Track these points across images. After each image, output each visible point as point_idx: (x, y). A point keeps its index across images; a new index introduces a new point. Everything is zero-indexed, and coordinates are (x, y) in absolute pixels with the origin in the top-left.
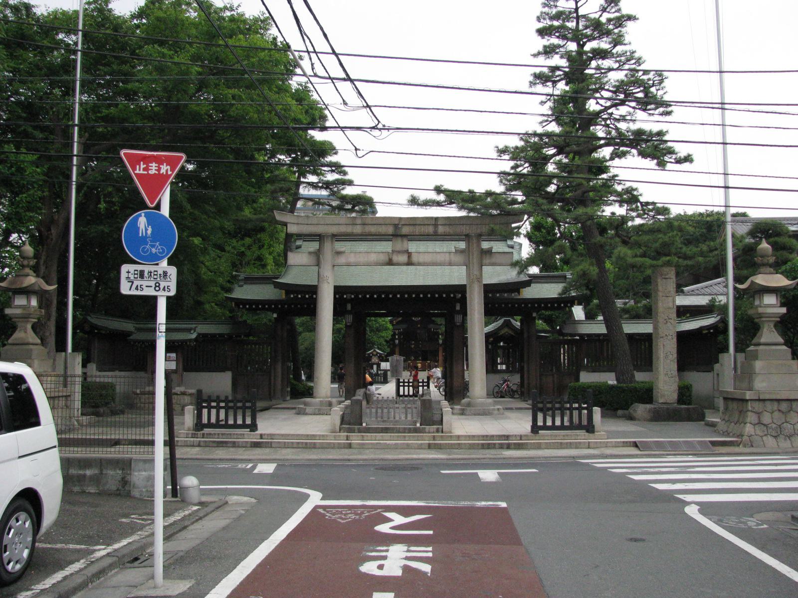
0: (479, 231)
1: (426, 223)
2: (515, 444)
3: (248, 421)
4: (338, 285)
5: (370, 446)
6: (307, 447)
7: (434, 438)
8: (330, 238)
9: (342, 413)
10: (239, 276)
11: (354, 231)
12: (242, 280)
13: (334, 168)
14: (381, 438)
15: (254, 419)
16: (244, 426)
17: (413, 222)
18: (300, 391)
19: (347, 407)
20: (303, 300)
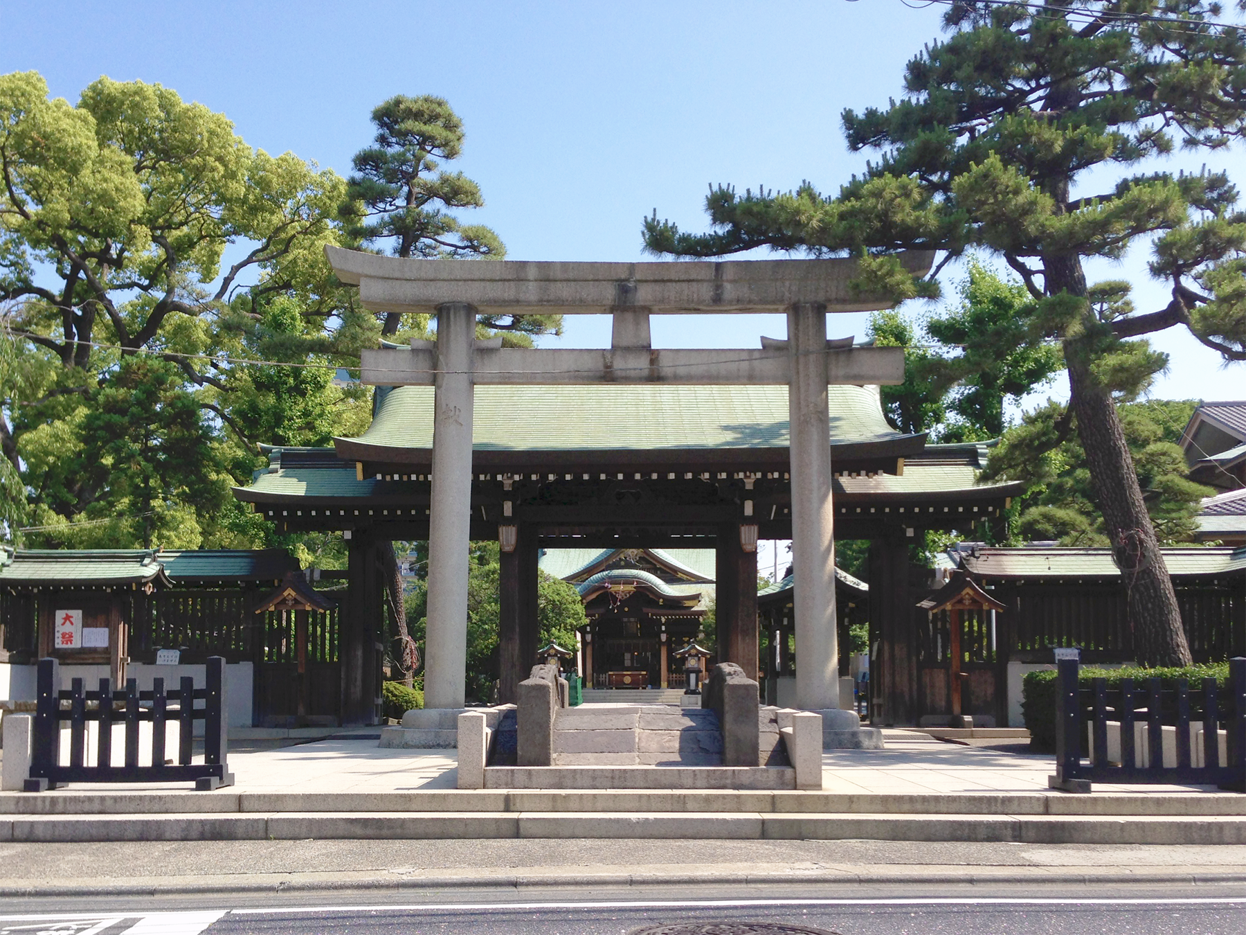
0: (821, 297)
1: (693, 276)
17: (659, 277)
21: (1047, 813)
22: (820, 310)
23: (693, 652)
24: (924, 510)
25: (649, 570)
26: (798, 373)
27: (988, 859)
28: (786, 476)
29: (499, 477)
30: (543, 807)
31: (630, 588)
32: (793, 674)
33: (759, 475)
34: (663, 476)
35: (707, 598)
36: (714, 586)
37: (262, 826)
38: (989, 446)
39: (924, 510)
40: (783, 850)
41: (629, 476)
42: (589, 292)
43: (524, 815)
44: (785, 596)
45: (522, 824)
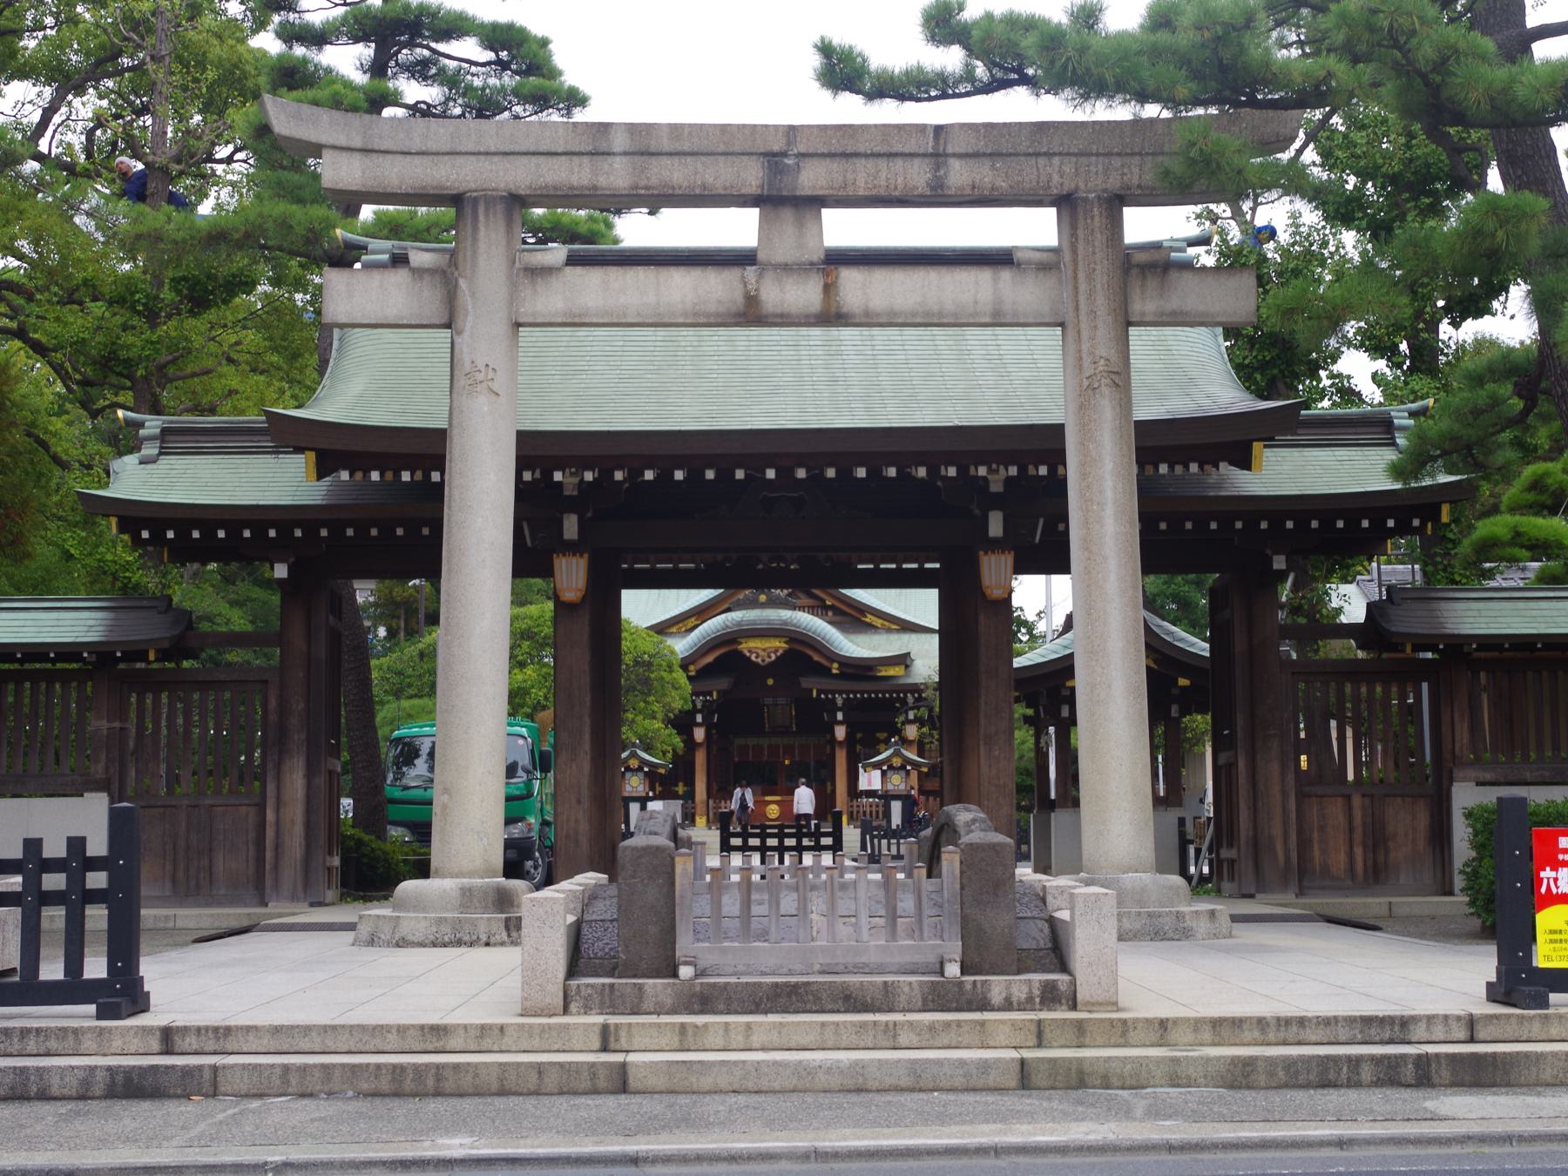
0: (1114, 183)
1: (898, 148)
2: (1453, 1058)
3: (96, 968)
4: (529, 426)
5: (723, 1081)
6: (401, 1086)
7: (1040, 1036)
8: (500, 208)
9: (571, 919)
10: (141, 425)
11: (602, 181)
12: (150, 438)
13: (504, 54)
14: (775, 1039)
15: (124, 952)
16: (72, 990)
17: (842, 144)
18: (371, 860)
19: (590, 897)
20: (388, 500)
21: (1472, 1040)
22: (1116, 202)
23: (897, 762)
24: (1302, 523)
25: (812, 610)
26: (1077, 309)
27: (1372, 1111)
28: (1060, 470)
29: (558, 476)
30: (663, 1043)
31: (779, 644)
32: (1076, 803)
33: (1013, 471)
34: (845, 473)
35: (926, 660)
36: (936, 638)
37: (207, 1075)
38: (1412, 414)
39: (1302, 523)
40: (1055, 1104)
41: (785, 473)
42: (718, 174)
43: (632, 1057)
44: (1062, 669)
45: (631, 1072)
